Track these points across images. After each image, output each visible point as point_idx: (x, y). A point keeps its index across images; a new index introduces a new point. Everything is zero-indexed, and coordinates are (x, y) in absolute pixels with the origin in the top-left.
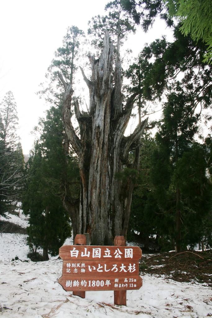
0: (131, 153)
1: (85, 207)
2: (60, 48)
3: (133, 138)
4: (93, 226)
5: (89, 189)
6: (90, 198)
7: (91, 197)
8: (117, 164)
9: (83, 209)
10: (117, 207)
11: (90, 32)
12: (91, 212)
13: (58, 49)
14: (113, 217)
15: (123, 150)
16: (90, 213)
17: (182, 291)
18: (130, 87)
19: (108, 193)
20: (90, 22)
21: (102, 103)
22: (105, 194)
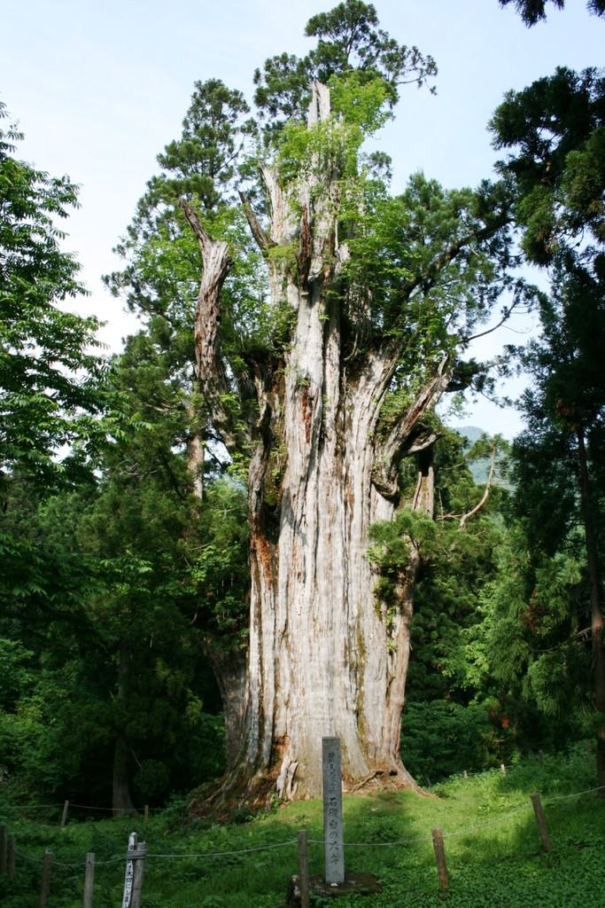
0: (564, 339)
1: (268, 639)
2: (172, 149)
3: (341, 488)
4: (298, 700)
5: (282, 579)
6: (285, 612)
7: (287, 609)
8: (366, 498)
9: (260, 645)
10: (369, 636)
11: (261, 99)
12: (289, 656)
13: (166, 148)
14: (356, 669)
15: (382, 453)
16: (286, 658)
17: (331, 629)
18: (423, 191)
19: (340, 594)
20: (258, 75)
21: (264, 581)
22: (330, 595)
